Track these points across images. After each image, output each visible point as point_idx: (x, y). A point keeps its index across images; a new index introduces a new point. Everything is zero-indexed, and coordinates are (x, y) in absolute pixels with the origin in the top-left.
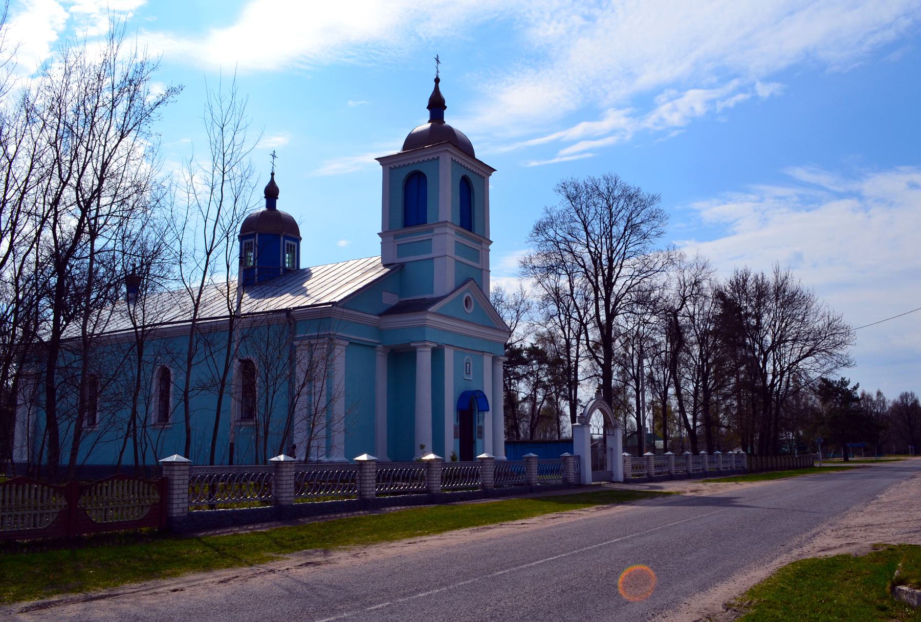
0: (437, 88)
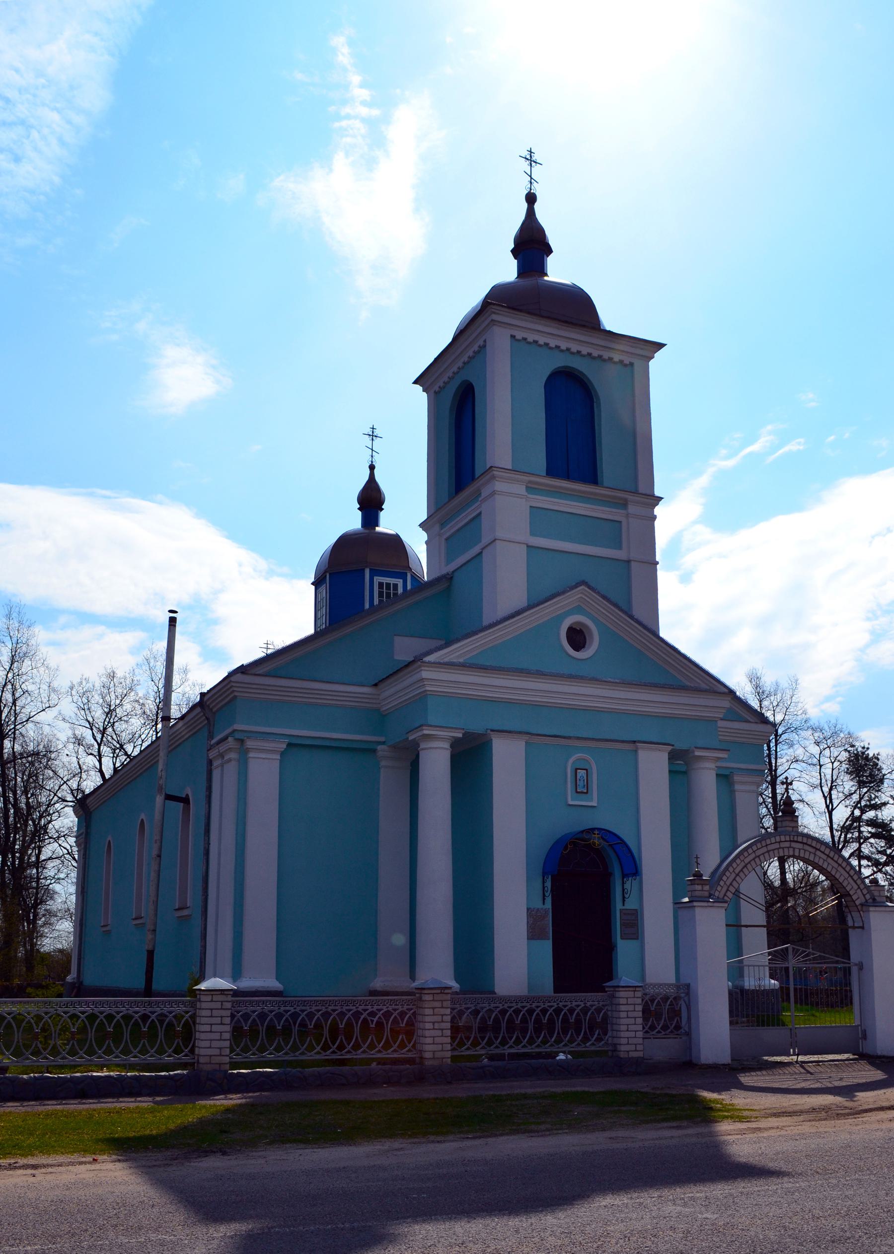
0: (531, 213)
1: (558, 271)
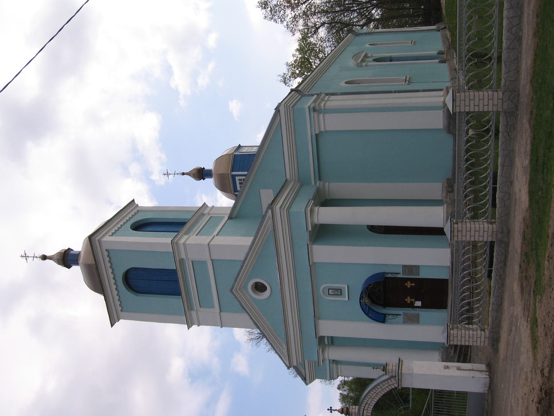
1: (78, 245)
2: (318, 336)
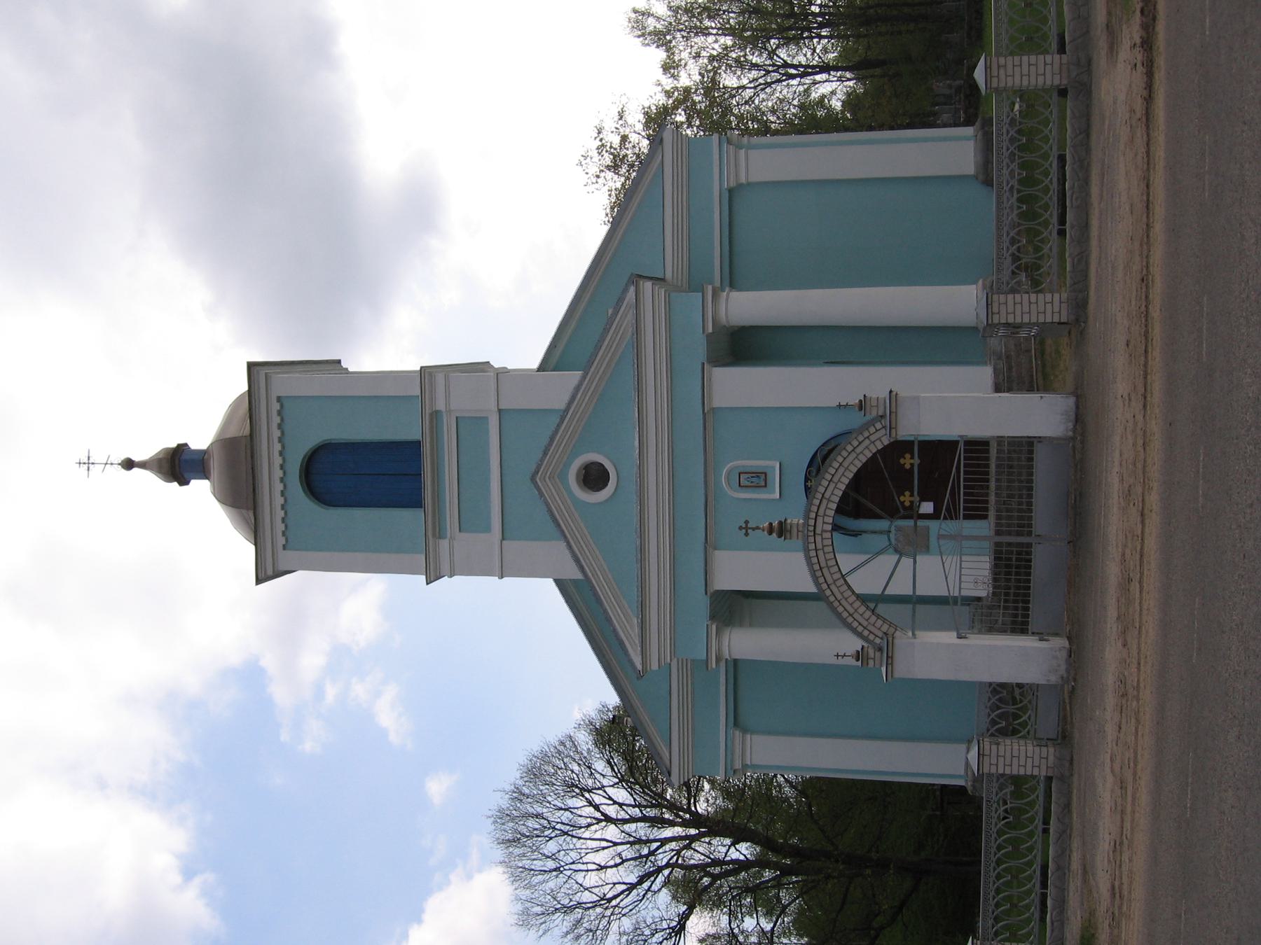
0: (143, 465)
2: (710, 590)
